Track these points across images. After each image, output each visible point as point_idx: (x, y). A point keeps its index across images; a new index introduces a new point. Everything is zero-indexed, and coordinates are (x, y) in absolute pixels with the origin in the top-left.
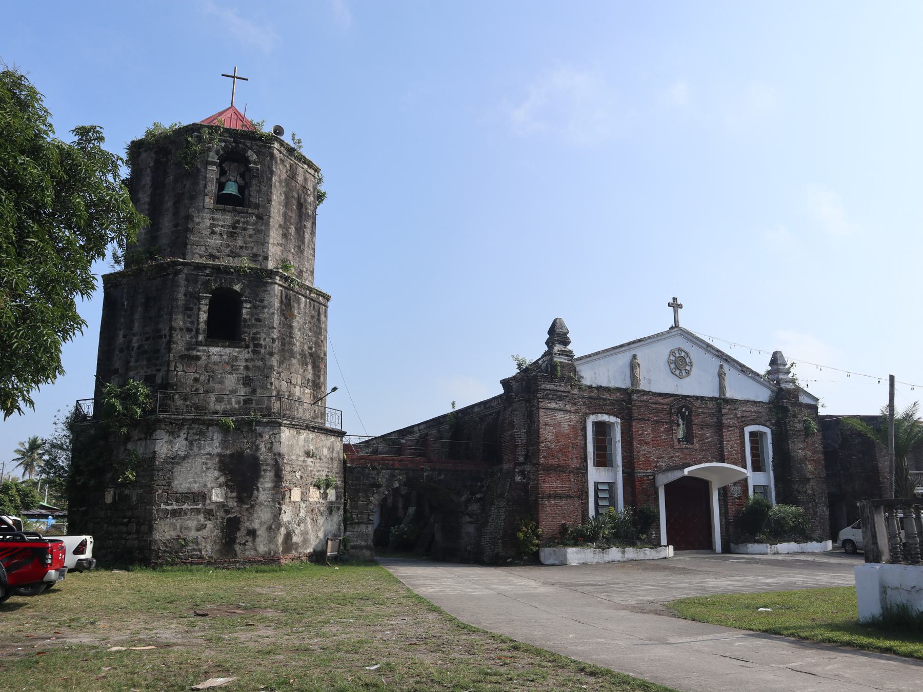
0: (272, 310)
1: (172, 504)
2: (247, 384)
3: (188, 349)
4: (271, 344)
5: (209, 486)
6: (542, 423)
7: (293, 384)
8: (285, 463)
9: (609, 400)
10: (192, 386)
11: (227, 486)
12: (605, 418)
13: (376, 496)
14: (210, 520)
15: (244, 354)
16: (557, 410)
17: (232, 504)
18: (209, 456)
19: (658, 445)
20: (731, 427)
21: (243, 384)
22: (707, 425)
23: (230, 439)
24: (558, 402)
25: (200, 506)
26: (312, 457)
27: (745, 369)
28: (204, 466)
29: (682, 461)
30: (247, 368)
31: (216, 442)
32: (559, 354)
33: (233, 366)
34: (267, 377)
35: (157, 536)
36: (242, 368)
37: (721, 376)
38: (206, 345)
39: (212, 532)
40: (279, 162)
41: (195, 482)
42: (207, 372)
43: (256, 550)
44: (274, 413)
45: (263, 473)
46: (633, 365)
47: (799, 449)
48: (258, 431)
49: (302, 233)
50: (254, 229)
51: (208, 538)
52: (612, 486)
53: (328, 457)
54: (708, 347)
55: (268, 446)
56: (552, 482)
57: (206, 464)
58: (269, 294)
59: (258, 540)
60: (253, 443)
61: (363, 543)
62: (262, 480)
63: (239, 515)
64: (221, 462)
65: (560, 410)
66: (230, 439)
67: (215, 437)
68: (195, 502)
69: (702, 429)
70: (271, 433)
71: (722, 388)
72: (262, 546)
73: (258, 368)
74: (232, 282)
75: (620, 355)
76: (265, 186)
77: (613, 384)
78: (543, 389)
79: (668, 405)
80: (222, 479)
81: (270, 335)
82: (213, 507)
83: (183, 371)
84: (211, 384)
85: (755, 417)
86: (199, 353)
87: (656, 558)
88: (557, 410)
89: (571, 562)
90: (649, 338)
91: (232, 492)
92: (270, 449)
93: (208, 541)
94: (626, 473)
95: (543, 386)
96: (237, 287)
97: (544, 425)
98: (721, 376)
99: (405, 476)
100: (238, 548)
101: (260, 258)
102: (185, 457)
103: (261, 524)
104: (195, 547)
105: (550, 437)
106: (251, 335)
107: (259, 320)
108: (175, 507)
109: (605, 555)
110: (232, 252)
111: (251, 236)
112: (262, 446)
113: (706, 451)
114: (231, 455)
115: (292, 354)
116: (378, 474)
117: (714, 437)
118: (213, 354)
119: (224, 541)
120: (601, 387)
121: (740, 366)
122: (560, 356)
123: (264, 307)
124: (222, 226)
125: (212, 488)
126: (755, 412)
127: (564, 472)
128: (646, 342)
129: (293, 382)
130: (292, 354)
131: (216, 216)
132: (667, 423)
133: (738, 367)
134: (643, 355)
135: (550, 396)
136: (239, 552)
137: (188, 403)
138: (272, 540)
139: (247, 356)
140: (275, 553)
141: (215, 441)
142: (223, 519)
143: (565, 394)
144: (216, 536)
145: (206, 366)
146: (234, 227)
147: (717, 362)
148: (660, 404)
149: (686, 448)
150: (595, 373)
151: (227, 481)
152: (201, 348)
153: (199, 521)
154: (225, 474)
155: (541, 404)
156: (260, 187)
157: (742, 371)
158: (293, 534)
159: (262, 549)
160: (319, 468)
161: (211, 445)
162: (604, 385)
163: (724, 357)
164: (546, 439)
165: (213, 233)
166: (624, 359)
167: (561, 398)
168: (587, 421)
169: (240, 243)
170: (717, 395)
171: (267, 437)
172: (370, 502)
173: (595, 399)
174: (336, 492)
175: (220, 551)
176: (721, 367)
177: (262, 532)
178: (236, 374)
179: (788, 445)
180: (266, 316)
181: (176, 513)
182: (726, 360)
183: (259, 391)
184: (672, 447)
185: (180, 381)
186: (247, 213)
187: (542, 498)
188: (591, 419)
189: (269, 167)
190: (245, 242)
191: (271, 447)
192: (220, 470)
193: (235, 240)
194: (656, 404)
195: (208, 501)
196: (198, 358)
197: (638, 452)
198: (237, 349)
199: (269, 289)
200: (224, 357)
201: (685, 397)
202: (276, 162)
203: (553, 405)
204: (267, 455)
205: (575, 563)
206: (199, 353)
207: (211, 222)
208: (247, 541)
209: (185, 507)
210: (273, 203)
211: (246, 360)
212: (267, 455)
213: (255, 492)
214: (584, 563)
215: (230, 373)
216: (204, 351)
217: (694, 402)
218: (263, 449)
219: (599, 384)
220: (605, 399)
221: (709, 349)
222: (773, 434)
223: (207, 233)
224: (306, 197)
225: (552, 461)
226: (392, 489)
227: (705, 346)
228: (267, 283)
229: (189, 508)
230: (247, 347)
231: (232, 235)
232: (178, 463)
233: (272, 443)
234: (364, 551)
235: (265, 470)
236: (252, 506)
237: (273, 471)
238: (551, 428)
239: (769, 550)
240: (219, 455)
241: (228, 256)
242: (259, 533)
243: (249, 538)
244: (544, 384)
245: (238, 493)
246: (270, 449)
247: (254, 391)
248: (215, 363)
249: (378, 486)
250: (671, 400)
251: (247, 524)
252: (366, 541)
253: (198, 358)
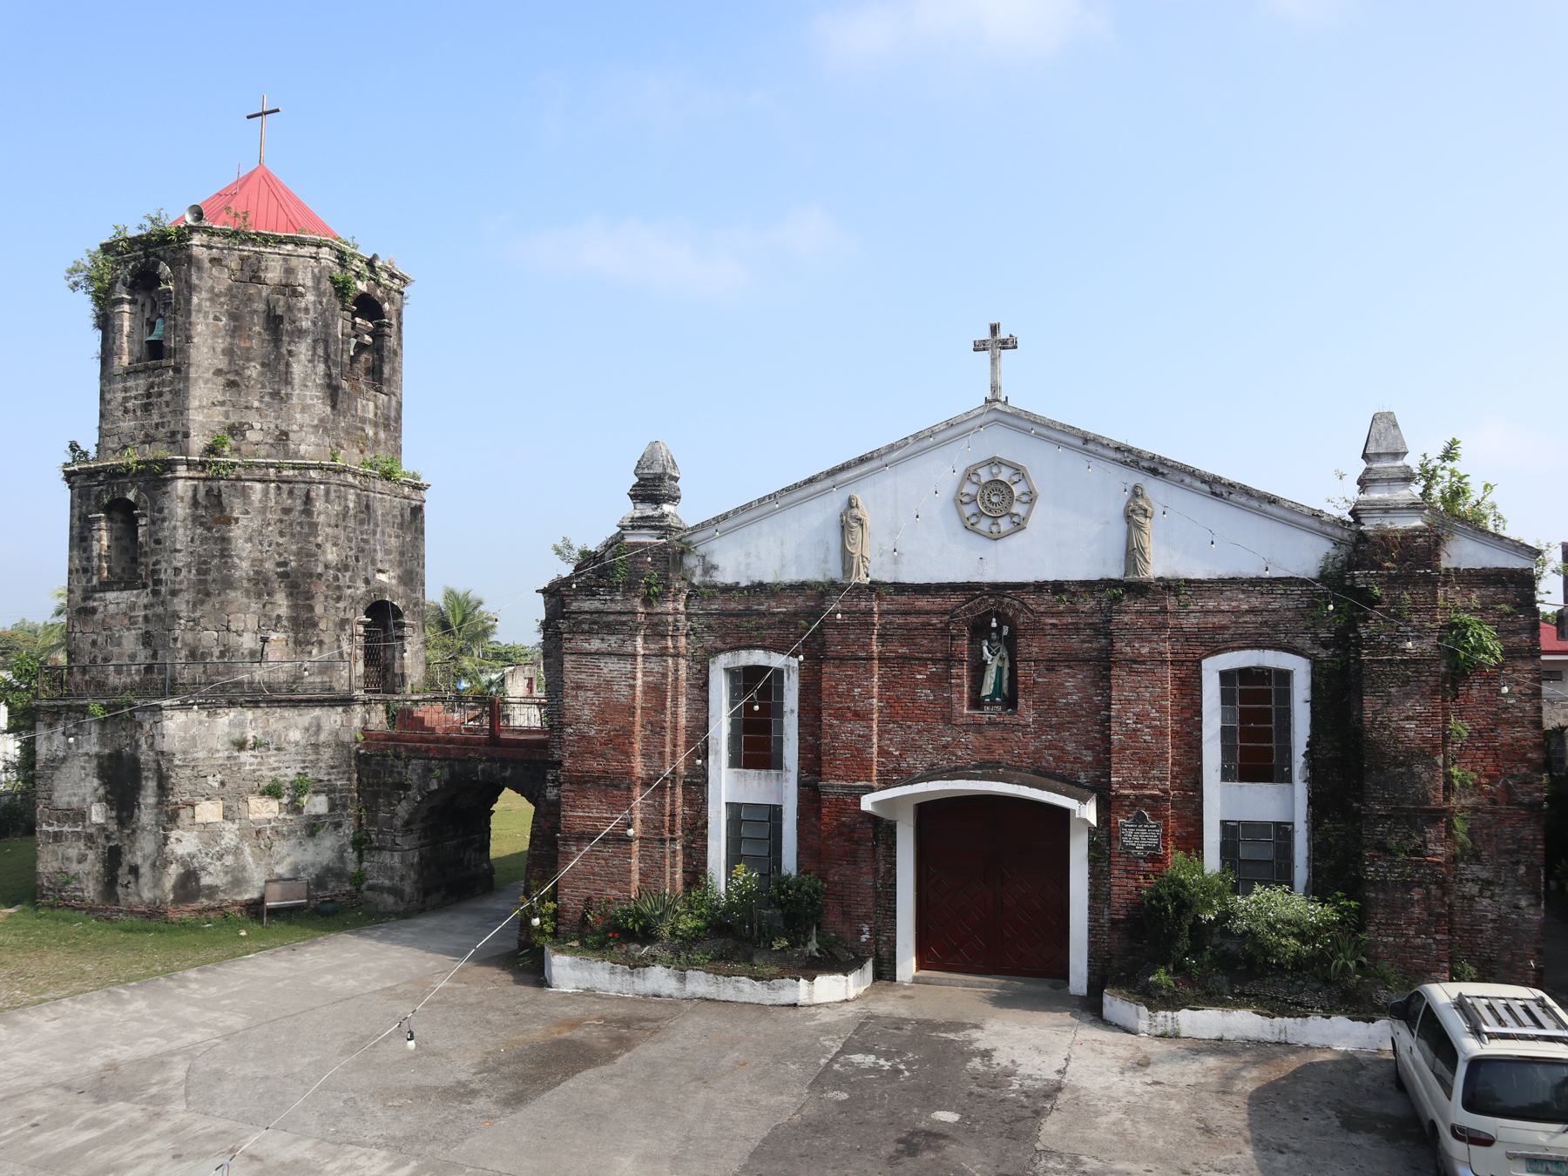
0: (173, 523)
1: (52, 825)
2: (148, 643)
3: (85, 599)
4: (173, 578)
5: (88, 800)
6: (568, 683)
7: (236, 632)
8: (177, 766)
9: (774, 614)
10: (90, 653)
11: (108, 801)
12: (758, 658)
13: (404, 803)
14: (91, 848)
15: (144, 598)
16: (603, 654)
17: (113, 827)
18: (87, 758)
19: (906, 718)
20: (1143, 662)
21: (143, 644)
22: (1072, 660)
23: (108, 731)
24: (606, 637)
25: (79, 829)
26: (253, 749)
27: (1218, 490)
28: (83, 772)
29: (978, 757)
30: (146, 618)
31: (94, 737)
32: (633, 528)
33: (131, 617)
34: (169, 630)
35: (40, 868)
36: (141, 619)
37: (1134, 516)
38: (101, 591)
39: (94, 866)
40: (207, 265)
41: (75, 795)
42: (104, 630)
43: (139, 896)
44: (183, 684)
45: (144, 783)
46: (849, 522)
47: (1408, 718)
48: (137, 719)
49: (282, 368)
50: (171, 391)
51: (89, 874)
52: (775, 812)
53: (303, 742)
54: (1088, 443)
55: (150, 741)
56: (588, 806)
57: (84, 768)
58: (170, 496)
59: (142, 881)
60: (132, 737)
61: (387, 883)
62: (143, 792)
63: (120, 844)
64: (100, 766)
65: (610, 654)
66: (108, 731)
67: (93, 730)
68: (75, 823)
69: (1051, 669)
70: (151, 721)
71: (1133, 554)
72: (146, 890)
73: (159, 618)
74: (125, 490)
75: (814, 502)
76: (182, 316)
77: (791, 576)
78: (576, 613)
79: (944, 613)
80: (101, 791)
81: (171, 562)
82: (92, 830)
83: (81, 631)
84: (110, 648)
85: (1251, 629)
86: (95, 604)
87: (768, 1003)
88: (603, 654)
89: (560, 983)
90: (892, 448)
91: (112, 809)
92: (151, 746)
93: (90, 877)
94: (804, 786)
95: (574, 606)
96: (131, 496)
97: (573, 688)
98: (1134, 516)
99: (447, 770)
100: (120, 890)
101: (179, 437)
102: (64, 759)
103: (145, 858)
104: (78, 886)
105: (587, 714)
106: (151, 567)
107: (158, 542)
108: (57, 829)
109: (636, 979)
110: (147, 435)
111: (167, 404)
112: (143, 741)
113: (1059, 728)
114: (110, 755)
115: (228, 583)
116: (406, 766)
117: (1092, 691)
118: (111, 603)
119: (106, 879)
120: (761, 585)
121: (1204, 482)
122: (636, 531)
123: (164, 520)
124: (135, 398)
125: (92, 803)
126: (1252, 611)
127: (617, 787)
128: (886, 459)
129: (233, 628)
130: (228, 583)
131: (128, 384)
132: (935, 661)
133: (1198, 484)
134: (873, 497)
135: (586, 627)
136: (121, 896)
137: (87, 677)
138: (157, 883)
139: (146, 601)
140: (161, 902)
141: (93, 735)
142: (104, 847)
143: (624, 618)
144: (98, 871)
145: (103, 621)
146: (149, 395)
147: (1121, 479)
148: (919, 613)
149: (991, 723)
150: (748, 555)
151: (107, 793)
152: (97, 595)
153: (79, 849)
154: (105, 784)
155: (567, 645)
156: (175, 320)
157: (1214, 493)
158: (203, 873)
159: (147, 895)
160: (276, 765)
161: (88, 741)
162: (768, 579)
163: (1145, 464)
164: (578, 719)
165: (126, 411)
166: (823, 512)
167: (610, 628)
168: (712, 668)
169: (156, 419)
170: (1116, 573)
171: (148, 727)
172: (394, 814)
173: (738, 615)
174: (330, 799)
175: (101, 893)
176: (1136, 493)
177: (145, 870)
178: (135, 629)
179: (1361, 708)
180: (167, 533)
181: (57, 837)
182: (1154, 472)
183: (160, 652)
184: (948, 720)
185: (78, 646)
186: (161, 367)
187: (565, 839)
188: (724, 660)
189: (186, 282)
190: (162, 417)
191: (153, 743)
192: (100, 777)
193: (150, 415)
194: (905, 613)
195: (88, 823)
196: (94, 611)
197: (835, 737)
198: (135, 592)
199: (169, 489)
200: (121, 606)
201: (998, 589)
202: (200, 269)
203: (596, 644)
204: (148, 755)
205: (568, 988)
206: (95, 604)
207: (123, 394)
208: (129, 883)
209: (66, 829)
210: (195, 340)
211: (146, 607)
212: (148, 755)
213: (136, 810)
214: (588, 990)
215: (129, 629)
216: (101, 599)
217: (1031, 600)
218: (144, 747)
219: (757, 580)
220: (761, 614)
221: (1090, 446)
222: (1314, 673)
223: (120, 414)
224: (293, 301)
225: (595, 765)
226: (428, 793)
227: (1079, 443)
228: (167, 480)
229: (70, 830)
230: (145, 586)
231: (146, 408)
232: (57, 768)
233: (153, 736)
234: (385, 895)
235: (147, 778)
236: (134, 831)
237: (156, 779)
238: (590, 694)
239: (1143, 1024)
240: (97, 756)
241: (144, 442)
242: (142, 871)
243: (131, 878)
244: (576, 600)
245: (119, 811)
246: (151, 746)
247: (155, 655)
248: (112, 617)
249: (407, 788)
250: (955, 599)
251: (129, 857)
252: (391, 878)
253: (94, 611)
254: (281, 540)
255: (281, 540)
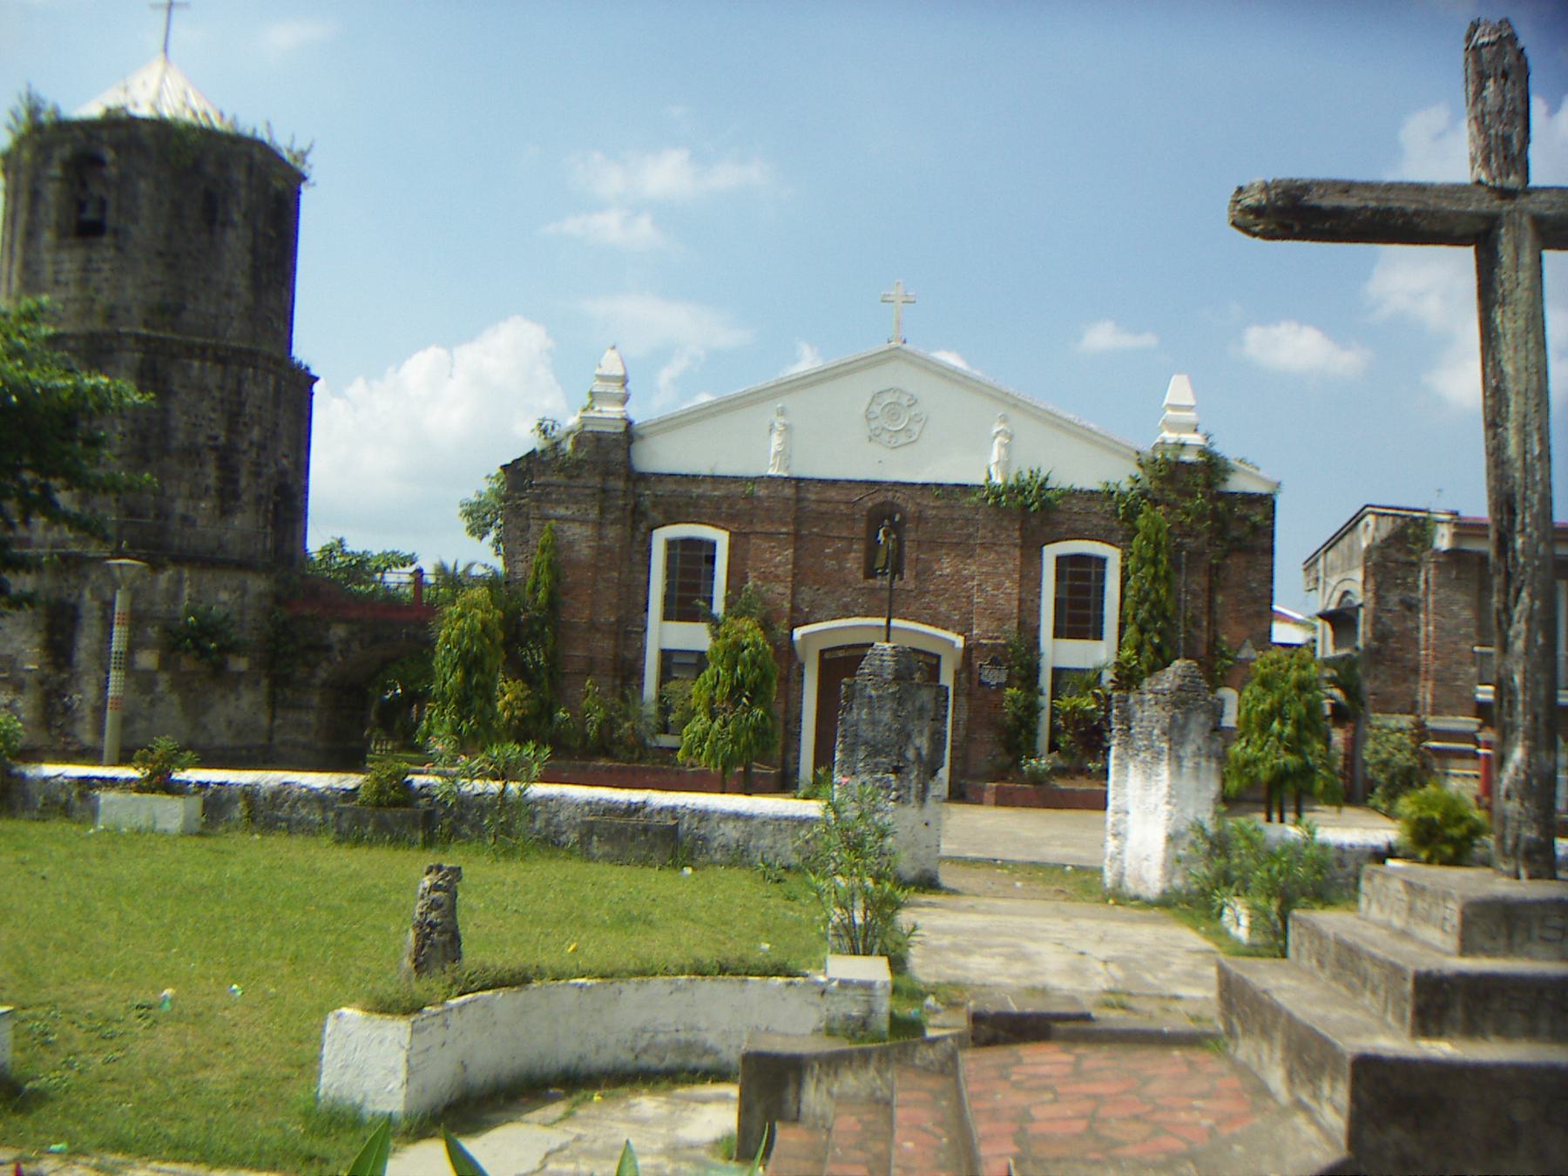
254: (213, 416)
255: (213, 416)
